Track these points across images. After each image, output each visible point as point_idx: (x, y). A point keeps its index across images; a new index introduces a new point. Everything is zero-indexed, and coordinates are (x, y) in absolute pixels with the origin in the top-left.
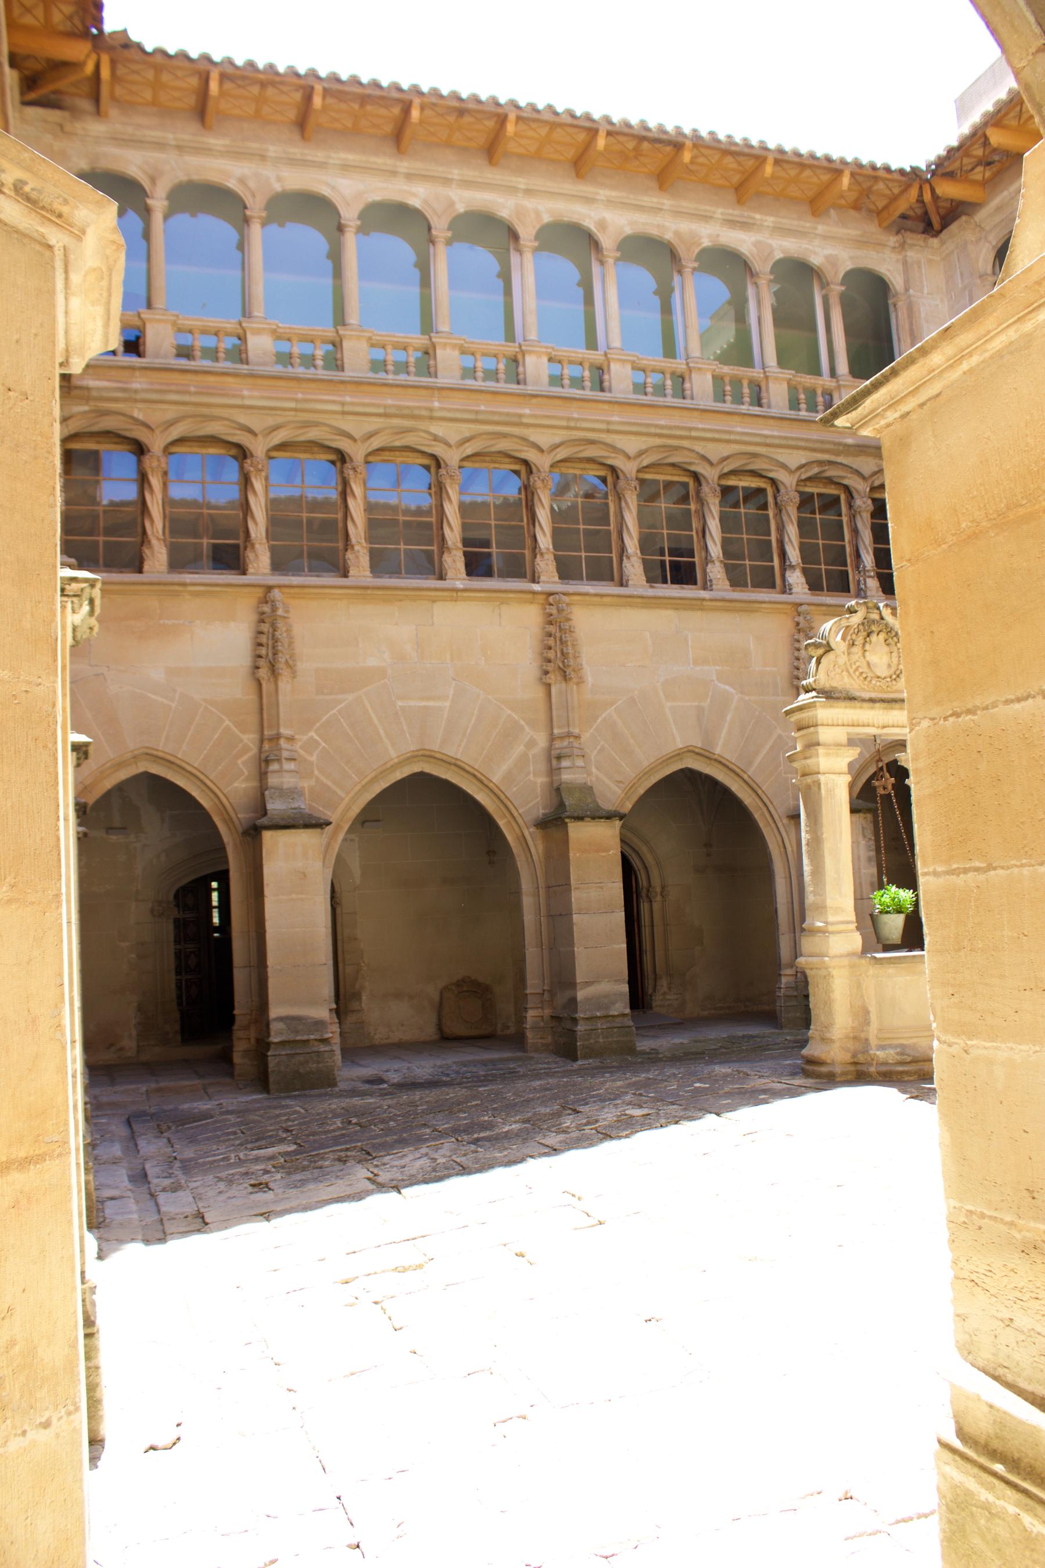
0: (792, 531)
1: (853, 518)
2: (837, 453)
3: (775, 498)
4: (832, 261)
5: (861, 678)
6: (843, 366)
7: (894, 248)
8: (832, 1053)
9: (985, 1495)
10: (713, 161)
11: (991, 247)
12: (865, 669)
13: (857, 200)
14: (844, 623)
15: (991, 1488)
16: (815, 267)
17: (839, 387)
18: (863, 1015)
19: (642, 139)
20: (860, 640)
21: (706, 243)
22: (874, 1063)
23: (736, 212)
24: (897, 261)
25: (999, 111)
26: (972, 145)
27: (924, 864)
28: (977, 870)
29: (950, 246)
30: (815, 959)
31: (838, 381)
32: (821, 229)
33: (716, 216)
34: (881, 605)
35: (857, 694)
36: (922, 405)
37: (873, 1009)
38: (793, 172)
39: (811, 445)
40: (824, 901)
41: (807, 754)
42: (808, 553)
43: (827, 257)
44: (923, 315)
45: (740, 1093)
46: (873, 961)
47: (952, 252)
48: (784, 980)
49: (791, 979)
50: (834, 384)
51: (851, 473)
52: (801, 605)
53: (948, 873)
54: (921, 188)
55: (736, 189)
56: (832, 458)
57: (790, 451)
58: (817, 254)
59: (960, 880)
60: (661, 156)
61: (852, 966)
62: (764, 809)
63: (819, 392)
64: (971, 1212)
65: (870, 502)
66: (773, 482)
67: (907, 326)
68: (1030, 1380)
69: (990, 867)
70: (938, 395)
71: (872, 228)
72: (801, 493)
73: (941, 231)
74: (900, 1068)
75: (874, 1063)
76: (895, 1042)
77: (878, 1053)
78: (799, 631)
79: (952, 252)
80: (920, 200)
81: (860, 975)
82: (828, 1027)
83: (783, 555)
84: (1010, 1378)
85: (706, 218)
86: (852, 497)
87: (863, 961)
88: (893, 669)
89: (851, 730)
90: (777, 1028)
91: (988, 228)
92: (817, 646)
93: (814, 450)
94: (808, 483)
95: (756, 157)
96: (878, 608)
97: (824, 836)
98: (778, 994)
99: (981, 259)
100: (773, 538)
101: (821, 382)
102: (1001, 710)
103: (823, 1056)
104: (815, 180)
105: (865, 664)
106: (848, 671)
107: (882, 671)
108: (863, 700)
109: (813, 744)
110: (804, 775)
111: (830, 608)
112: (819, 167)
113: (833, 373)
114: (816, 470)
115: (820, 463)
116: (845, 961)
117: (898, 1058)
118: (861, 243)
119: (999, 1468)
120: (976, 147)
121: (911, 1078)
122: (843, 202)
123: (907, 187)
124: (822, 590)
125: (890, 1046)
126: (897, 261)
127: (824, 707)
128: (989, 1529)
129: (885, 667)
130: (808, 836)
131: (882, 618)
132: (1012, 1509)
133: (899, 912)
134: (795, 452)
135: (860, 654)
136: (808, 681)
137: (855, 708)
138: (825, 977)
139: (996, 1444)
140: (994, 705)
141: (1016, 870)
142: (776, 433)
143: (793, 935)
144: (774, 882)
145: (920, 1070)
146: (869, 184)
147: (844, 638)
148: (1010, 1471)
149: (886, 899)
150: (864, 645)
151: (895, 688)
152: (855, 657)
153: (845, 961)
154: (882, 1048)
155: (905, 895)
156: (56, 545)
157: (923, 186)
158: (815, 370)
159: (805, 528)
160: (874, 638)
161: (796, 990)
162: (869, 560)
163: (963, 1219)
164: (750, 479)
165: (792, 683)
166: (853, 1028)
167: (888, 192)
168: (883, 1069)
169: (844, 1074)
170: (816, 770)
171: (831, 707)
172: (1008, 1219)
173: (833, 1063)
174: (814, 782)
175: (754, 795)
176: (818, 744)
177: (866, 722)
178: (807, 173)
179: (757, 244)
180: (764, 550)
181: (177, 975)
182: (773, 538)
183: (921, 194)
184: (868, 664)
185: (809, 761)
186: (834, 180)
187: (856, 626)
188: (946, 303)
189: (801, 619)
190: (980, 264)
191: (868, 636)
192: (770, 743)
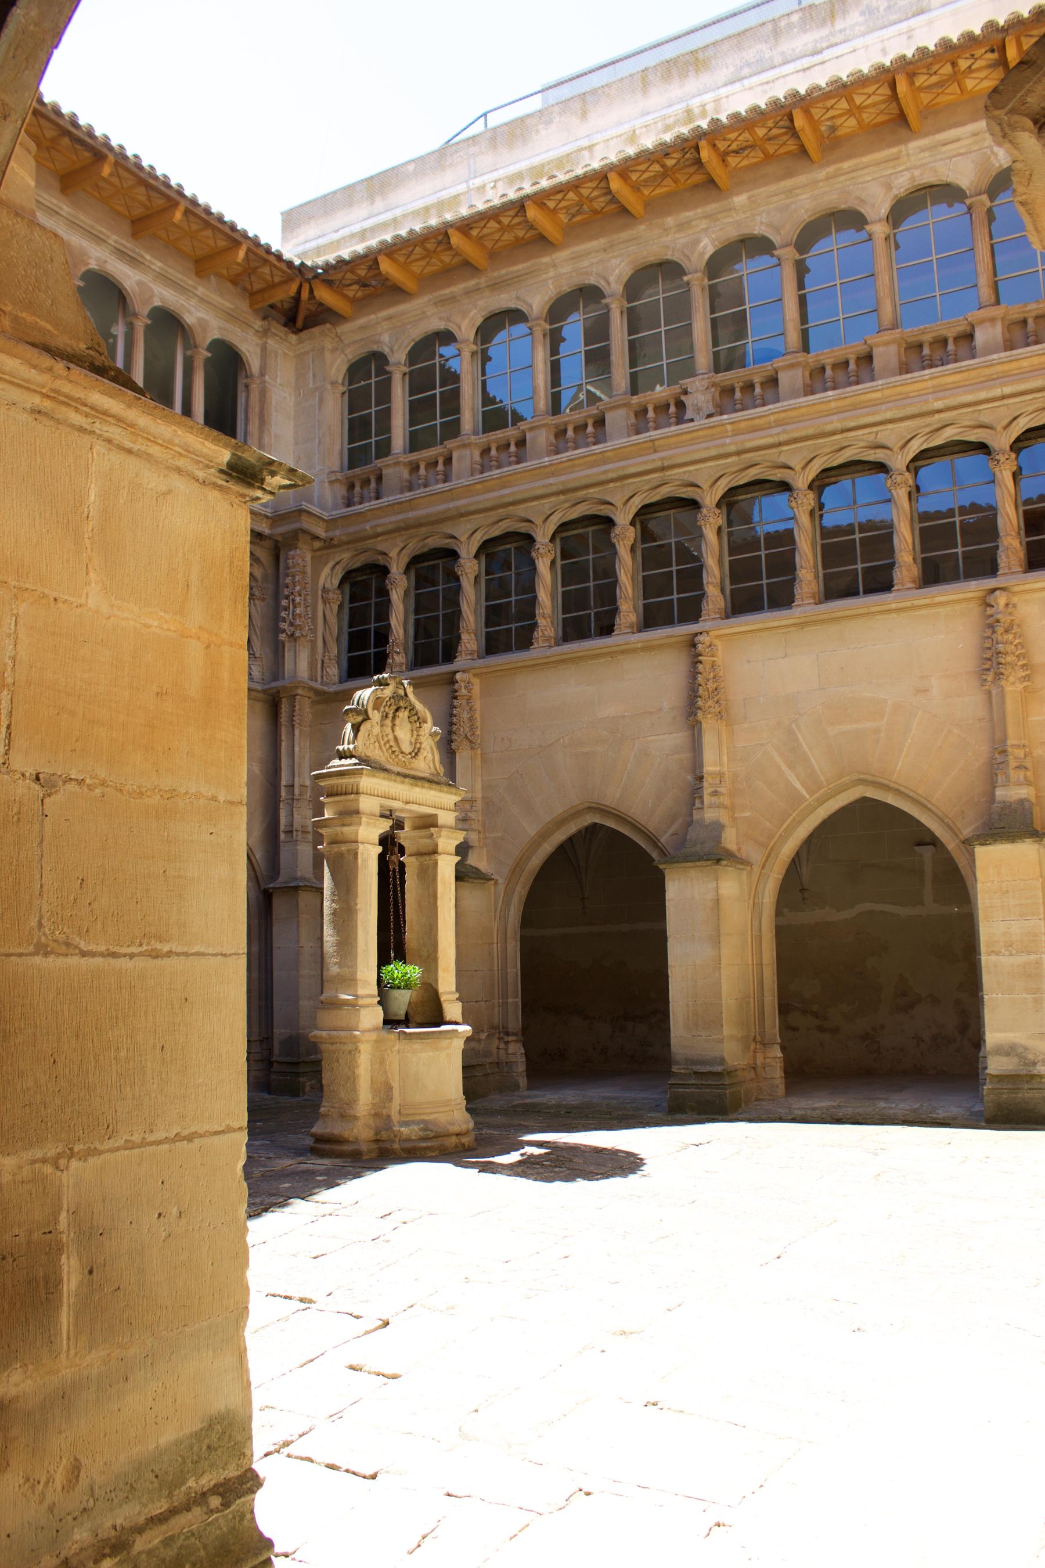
4: (204, 325)
5: (390, 751)
7: (258, 331)
8: (355, 1130)
10: (125, 186)
11: (346, 359)
13: (238, 275)
16: (186, 326)
18: (384, 1091)
19: (66, 133)
21: (93, 265)
22: (397, 1139)
23: (128, 245)
24: (257, 344)
25: (395, 245)
26: (360, 264)
29: (307, 346)
30: (342, 1033)
32: (201, 290)
33: (482, 286)
34: (405, 682)
37: (395, 1085)
38: (195, 227)
41: (348, 820)
43: (200, 320)
44: (274, 403)
46: (402, 1036)
47: (307, 353)
54: (301, 286)
55: (133, 222)
58: (193, 314)
60: (75, 158)
67: (257, 409)
71: (244, 306)
73: (301, 330)
74: (424, 1144)
75: (397, 1139)
76: (418, 1118)
77: (402, 1129)
79: (307, 353)
80: (297, 298)
81: (386, 1050)
82: (352, 1102)
85: (99, 240)
87: (392, 1036)
91: (346, 342)
95: (169, 198)
97: (358, 906)
99: (335, 367)
103: (346, 1134)
104: (211, 242)
112: (220, 230)
116: (373, 1036)
117: (421, 1133)
118: (231, 316)
120: (363, 267)
121: (434, 1154)
122: (225, 272)
123: (290, 280)
125: (413, 1122)
126: (257, 344)
127: (368, 775)
131: (406, 695)
137: (390, 780)
138: (350, 1052)
145: (442, 1145)
146: (257, 264)
154: (406, 1124)
157: (304, 284)
160: (400, 714)
167: (270, 278)
168: (408, 1145)
169: (370, 1151)
170: (353, 837)
171: (374, 776)
173: (356, 1141)
174: (349, 851)
178: (208, 233)
179: (140, 284)
183: (299, 292)
185: (345, 829)
186: (230, 248)
187: (388, 699)
188: (293, 398)
190: (333, 371)
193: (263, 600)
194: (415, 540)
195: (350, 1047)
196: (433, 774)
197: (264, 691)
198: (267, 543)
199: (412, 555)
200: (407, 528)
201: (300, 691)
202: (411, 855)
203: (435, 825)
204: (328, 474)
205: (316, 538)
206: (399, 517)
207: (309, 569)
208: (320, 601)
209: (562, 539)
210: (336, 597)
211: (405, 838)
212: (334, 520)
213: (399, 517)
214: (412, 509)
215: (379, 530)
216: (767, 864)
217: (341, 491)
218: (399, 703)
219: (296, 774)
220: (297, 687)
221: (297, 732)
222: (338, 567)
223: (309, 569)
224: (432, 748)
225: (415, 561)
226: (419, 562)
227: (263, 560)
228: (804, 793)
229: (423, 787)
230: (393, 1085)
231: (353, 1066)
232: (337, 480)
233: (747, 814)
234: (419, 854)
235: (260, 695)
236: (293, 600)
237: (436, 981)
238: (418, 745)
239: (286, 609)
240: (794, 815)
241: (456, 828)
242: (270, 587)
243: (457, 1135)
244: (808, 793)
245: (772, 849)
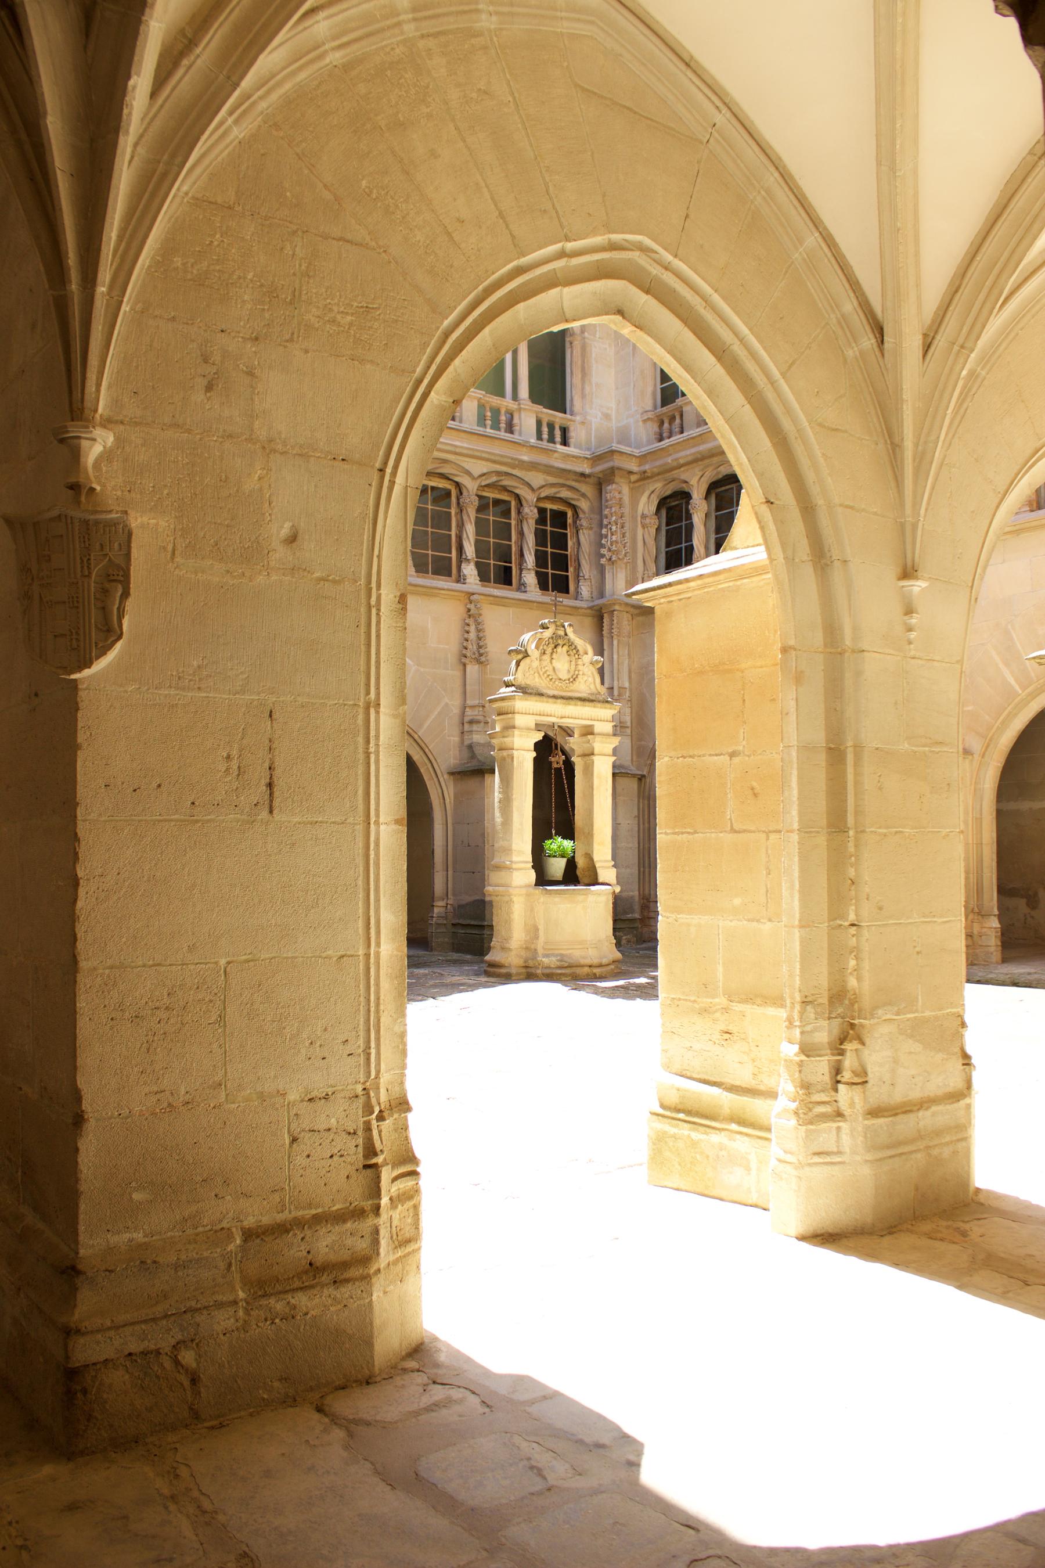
0: (470, 529)
1: (520, 522)
2: (513, 467)
3: (458, 499)
6: (524, 391)
9: (672, 1130)
12: (550, 672)
14: (539, 636)
15: (677, 1126)
17: (520, 410)
18: (534, 931)
20: (549, 650)
27: (660, 828)
28: (689, 833)
30: (501, 889)
31: (519, 404)
34: (566, 624)
35: (544, 691)
36: (680, 600)
37: (541, 927)
39: (493, 457)
40: (511, 846)
41: (506, 734)
42: (481, 549)
44: (594, 355)
45: (443, 986)
46: (544, 892)
48: (436, 910)
49: (442, 910)
50: (516, 407)
51: (523, 484)
52: (473, 594)
53: (673, 833)
56: (510, 470)
57: (474, 461)
59: (679, 837)
61: (528, 895)
62: (429, 765)
63: (503, 411)
64: (674, 999)
65: (536, 511)
66: (458, 485)
67: (580, 363)
68: (699, 1073)
69: (696, 832)
70: (689, 598)
72: (480, 497)
74: (559, 971)
76: (556, 952)
77: (544, 959)
78: (470, 616)
82: (508, 939)
83: (460, 549)
84: (689, 1074)
86: (522, 505)
87: (537, 892)
88: (572, 673)
89: (539, 718)
90: (427, 951)
92: (517, 652)
93: (494, 462)
94: (486, 489)
96: (564, 627)
97: (514, 796)
98: (430, 922)
100: (453, 533)
101: (505, 404)
102: (707, 759)
105: (551, 668)
106: (539, 673)
107: (564, 675)
108: (549, 697)
109: (510, 727)
110: (500, 749)
111: (497, 599)
113: (515, 397)
114: (494, 479)
115: (498, 473)
116: (524, 891)
117: (558, 963)
119: (681, 1116)
124: (489, 582)
125: (553, 955)
127: (520, 699)
128: (674, 1146)
129: (566, 672)
130: (501, 796)
131: (566, 634)
132: (686, 1133)
133: (563, 856)
134: (479, 462)
135: (548, 661)
136: (509, 678)
137: (543, 702)
139: (679, 1107)
140: (704, 756)
141: (708, 834)
142: (465, 445)
143: (445, 873)
144: (433, 828)
147: (537, 647)
148: (687, 1116)
149: (554, 847)
150: (552, 654)
151: (571, 688)
152: (545, 663)
153: (524, 891)
154: (547, 956)
155: (568, 844)
158: (501, 394)
159: (481, 526)
160: (559, 649)
161: (446, 919)
162: (531, 561)
163: (669, 1002)
164: (438, 480)
165: (460, 660)
166: (526, 941)
168: (548, 971)
169: (518, 974)
170: (511, 747)
171: (526, 700)
172: (693, 998)
173: (509, 966)
175: (421, 753)
176: (514, 727)
177: (549, 714)
180: (443, 543)
182: (453, 533)
184: (554, 669)
185: (506, 739)
189: (472, 606)
191: (555, 647)
192: (439, 709)
193: (591, 528)
194: (711, 469)
195: (506, 899)
196: (592, 694)
197: (591, 608)
198: (592, 480)
199: (710, 482)
200: (703, 459)
201: (617, 607)
202: (578, 756)
203: (592, 733)
204: (642, 414)
205: (630, 473)
206: (693, 450)
207: (626, 499)
208: (640, 526)
209: (717, 495)
210: (653, 522)
211: (574, 743)
212: (644, 456)
213: (693, 450)
214: (703, 443)
215: (682, 461)
216: (987, 753)
217: (654, 427)
218: (556, 642)
219: (615, 678)
220: (614, 604)
221: (615, 642)
222: (652, 495)
223: (626, 499)
224: (592, 674)
225: (713, 486)
226: (717, 487)
227: (589, 494)
228: (1017, 688)
229: (576, 705)
230: (540, 927)
231: (509, 913)
232: (648, 419)
233: (970, 708)
234: (584, 755)
235: (589, 611)
236: (611, 529)
237: (593, 852)
238: (577, 672)
239: (606, 537)
240: (1009, 708)
241: (614, 735)
242: (596, 517)
243: (590, 966)
244: (1021, 688)
245: (991, 740)
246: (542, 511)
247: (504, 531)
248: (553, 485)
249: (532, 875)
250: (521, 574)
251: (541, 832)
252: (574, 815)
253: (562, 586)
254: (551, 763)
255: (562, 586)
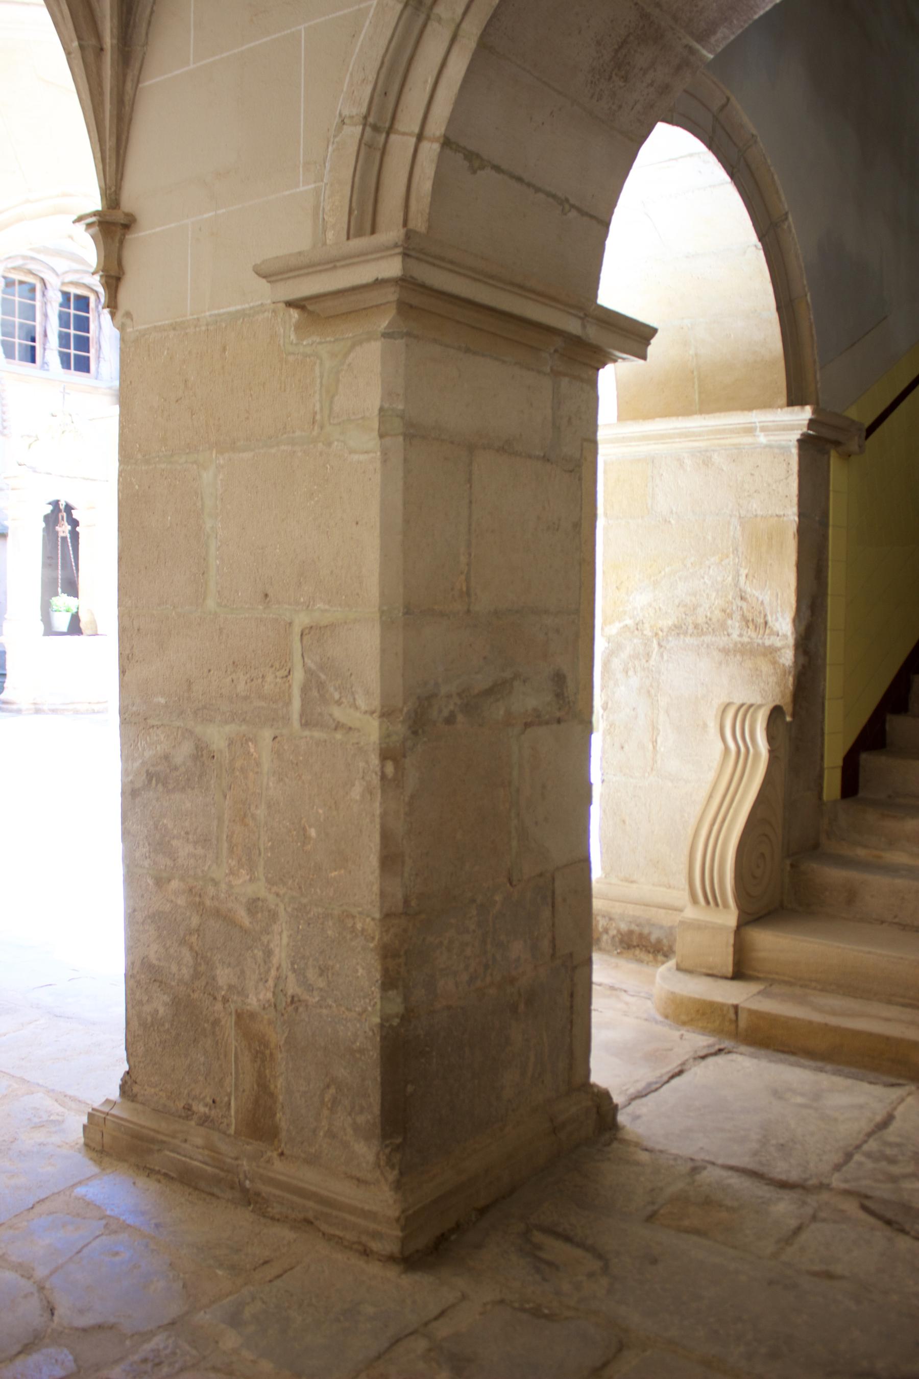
86: (46, 288)
133: (67, 611)
156: (605, 707)
181: (61, 326)
246: (66, 295)
247: (30, 312)
248: (76, 271)
249: (41, 627)
250: (44, 352)
251: (49, 590)
252: (78, 576)
253: (83, 365)
254: (57, 532)
255: (83, 365)
